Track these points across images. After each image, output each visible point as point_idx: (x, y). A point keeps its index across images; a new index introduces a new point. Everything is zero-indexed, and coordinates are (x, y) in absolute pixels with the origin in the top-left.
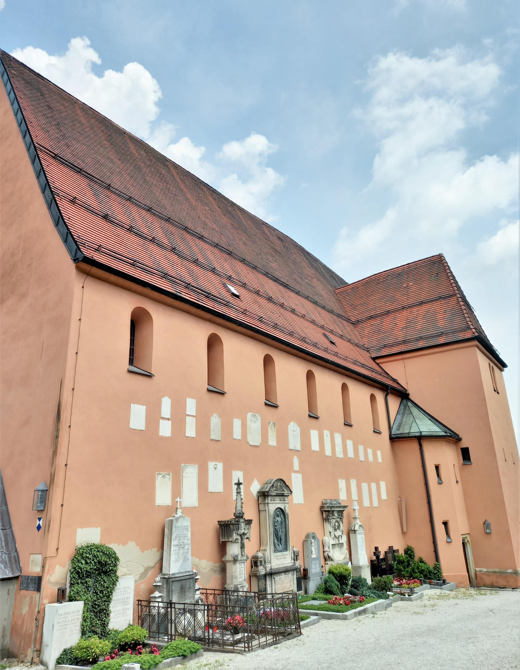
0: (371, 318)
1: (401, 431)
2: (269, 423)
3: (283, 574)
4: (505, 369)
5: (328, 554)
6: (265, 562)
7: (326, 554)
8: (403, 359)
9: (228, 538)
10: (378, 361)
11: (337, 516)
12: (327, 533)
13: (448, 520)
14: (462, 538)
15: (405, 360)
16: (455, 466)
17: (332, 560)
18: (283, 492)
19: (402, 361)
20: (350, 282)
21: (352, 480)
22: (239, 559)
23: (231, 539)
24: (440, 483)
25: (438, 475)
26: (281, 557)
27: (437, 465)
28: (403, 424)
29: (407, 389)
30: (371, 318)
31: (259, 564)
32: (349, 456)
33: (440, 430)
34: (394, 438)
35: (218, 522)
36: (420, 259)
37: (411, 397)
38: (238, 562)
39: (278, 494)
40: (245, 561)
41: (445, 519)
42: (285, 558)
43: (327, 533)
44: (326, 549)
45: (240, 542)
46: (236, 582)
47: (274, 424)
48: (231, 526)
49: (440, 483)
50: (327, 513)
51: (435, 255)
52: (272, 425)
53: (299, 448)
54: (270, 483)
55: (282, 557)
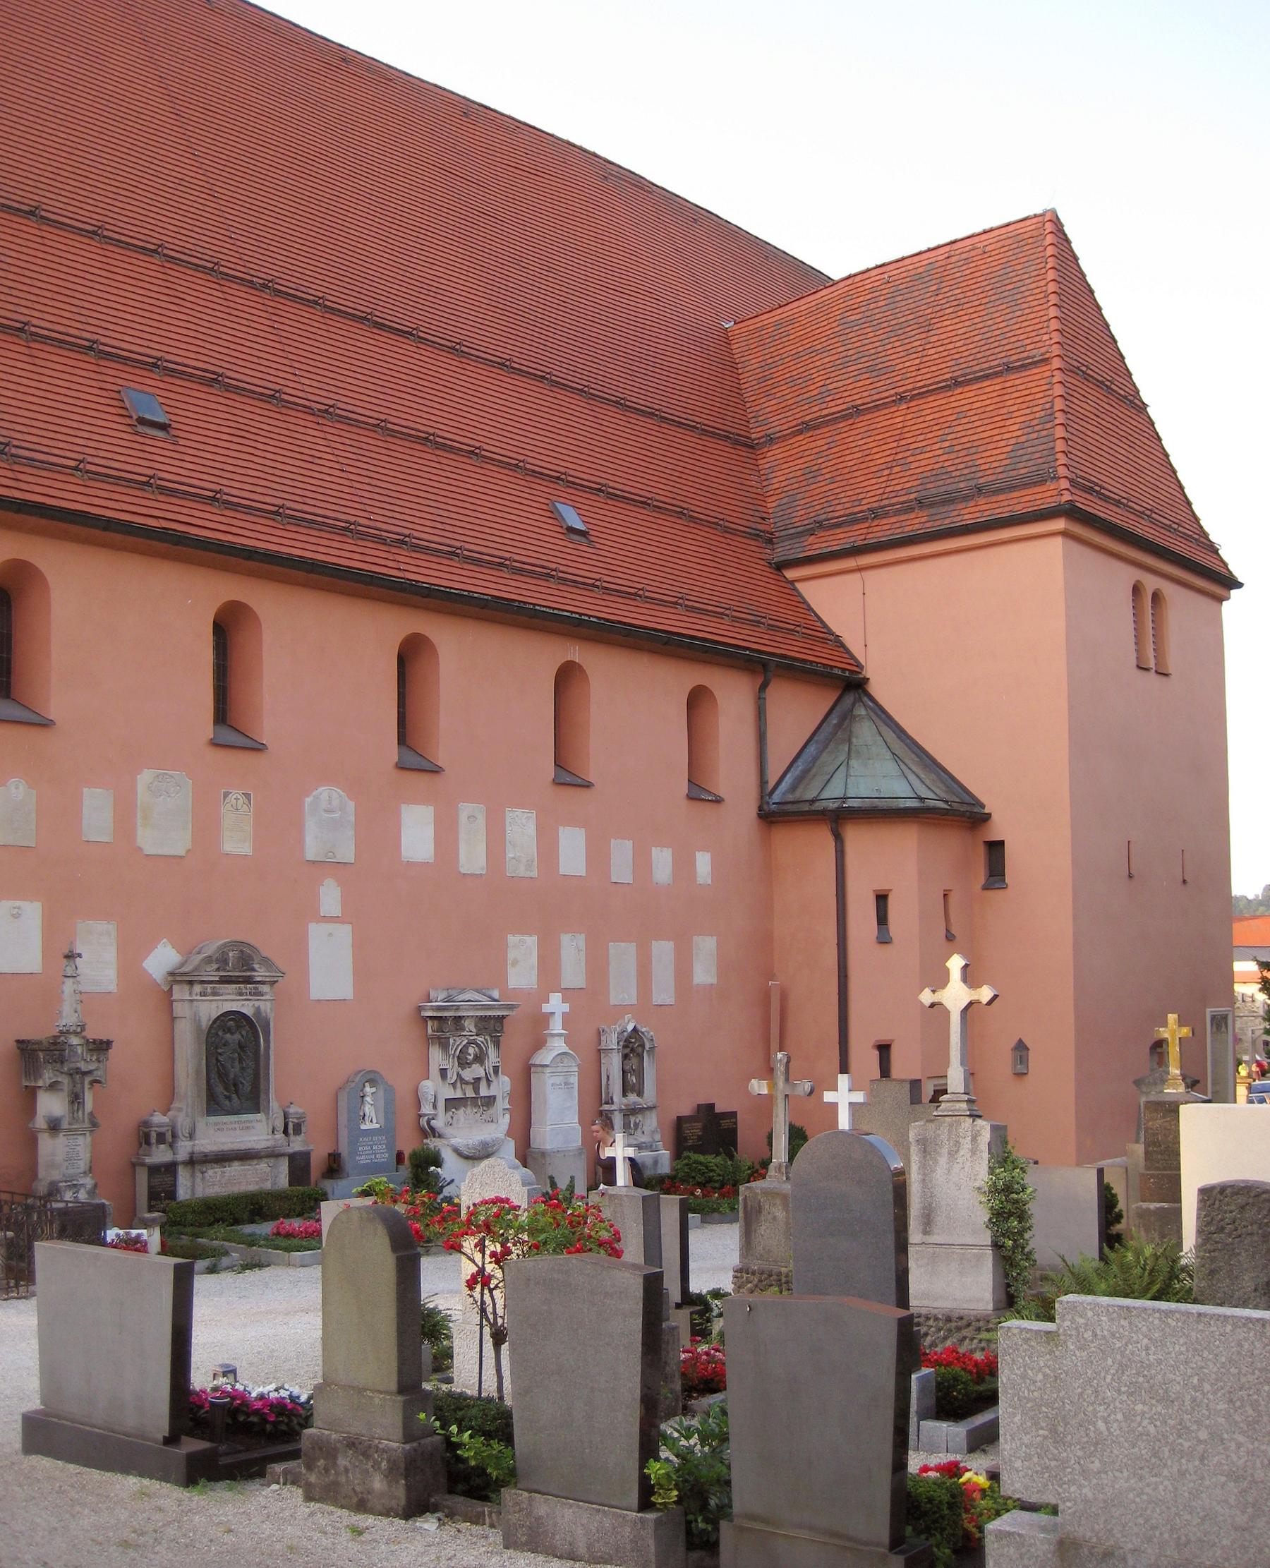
0: (807, 427)
1: (797, 795)
2: (226, 795)
3: (236, 1163)
4: (1234, 593)
5: (428, 1122)
6: (174, 1136)
7: (423, 1122)
8: (860, 569)
9: (36, 1080)
10: (790, 574)
11: (474, 1030)
12: (434, 1071)
13: (893, 1041)
14: (935, 1086)
15: (863, 573)
16: (953, 899)
17: (440, 1136)
18: (248, 974)
19: (857, 576)
20: (836, 275)
21: (565, 939)
22: (65, 1125)
23: (40, 1083)
24: (884, 939)
25: (882, 919)
26: (233, 1126)
27: (881, 893)
28: (814, 770)
29: (863, 664)
30: (807, 427)
31: (153, 1140)
32: (564, 869)
33: (825, 795)
34: (773, 814)
35: (18, 1041)
36: (987, 227)
37: (879, 688)
38: (61, 1134)
39: (224, 979)
40: (88, 1133)
41: (883, 1037)
42: (247, 1128)
43: (434, 1071)
44: (427, 1109)
45: (502, 1104)
46: (56, 1175)
47: (247, 796)
48: (41, 1055)
49: (884, 939)
50: (436, 1022)
51: (1031, 213)
52: (237, 799)
53: (347, 853)
54: (199, 953)
55: (237, 1126)
